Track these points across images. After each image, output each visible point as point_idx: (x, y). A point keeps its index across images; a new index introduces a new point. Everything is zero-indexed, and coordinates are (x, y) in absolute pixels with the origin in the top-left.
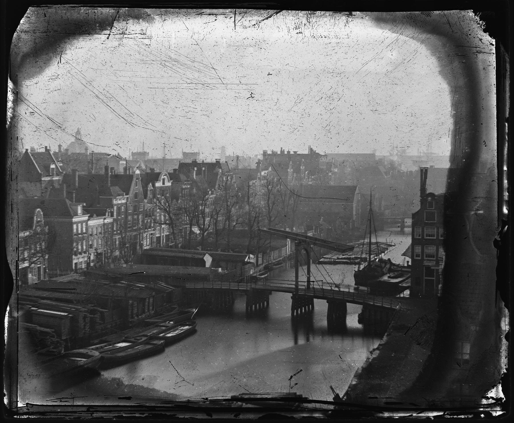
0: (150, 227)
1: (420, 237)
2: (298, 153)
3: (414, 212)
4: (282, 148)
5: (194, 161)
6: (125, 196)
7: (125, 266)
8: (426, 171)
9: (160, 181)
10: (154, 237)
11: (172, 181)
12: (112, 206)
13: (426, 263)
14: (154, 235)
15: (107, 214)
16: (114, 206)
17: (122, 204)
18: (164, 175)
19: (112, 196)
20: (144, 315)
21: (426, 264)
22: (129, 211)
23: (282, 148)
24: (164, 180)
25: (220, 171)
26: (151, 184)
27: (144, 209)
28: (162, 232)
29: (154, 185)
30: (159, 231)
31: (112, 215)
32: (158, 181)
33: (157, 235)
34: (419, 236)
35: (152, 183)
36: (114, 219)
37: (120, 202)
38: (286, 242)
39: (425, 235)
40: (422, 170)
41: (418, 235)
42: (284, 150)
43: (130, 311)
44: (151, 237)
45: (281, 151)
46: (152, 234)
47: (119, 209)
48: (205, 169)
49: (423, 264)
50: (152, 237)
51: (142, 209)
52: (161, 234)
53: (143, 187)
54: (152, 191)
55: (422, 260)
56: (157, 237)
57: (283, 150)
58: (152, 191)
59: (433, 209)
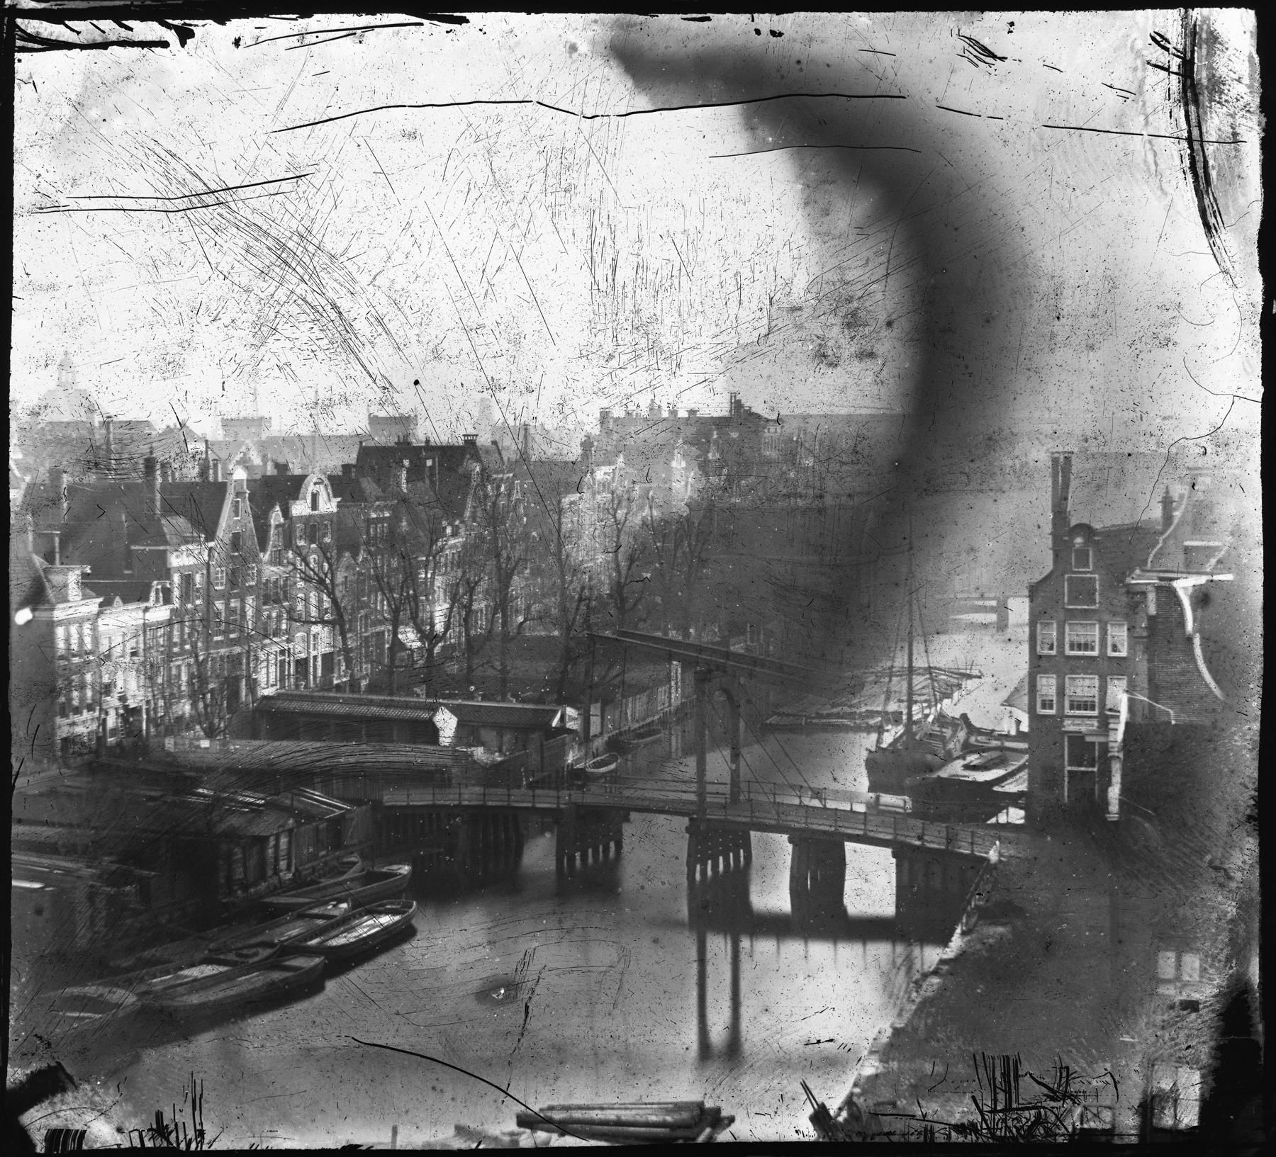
1: (1054, 652)
11: (339, 499)
12: (166, 573)
13: (1069, 726)
16: (172, 571)
18: (315, 484)
19: (166, 543)
21: (1072, 728)
26: (278, 508)
27: (259, 582)
29: (286, 512)
39: (1067, 646)
58: (280, 529)
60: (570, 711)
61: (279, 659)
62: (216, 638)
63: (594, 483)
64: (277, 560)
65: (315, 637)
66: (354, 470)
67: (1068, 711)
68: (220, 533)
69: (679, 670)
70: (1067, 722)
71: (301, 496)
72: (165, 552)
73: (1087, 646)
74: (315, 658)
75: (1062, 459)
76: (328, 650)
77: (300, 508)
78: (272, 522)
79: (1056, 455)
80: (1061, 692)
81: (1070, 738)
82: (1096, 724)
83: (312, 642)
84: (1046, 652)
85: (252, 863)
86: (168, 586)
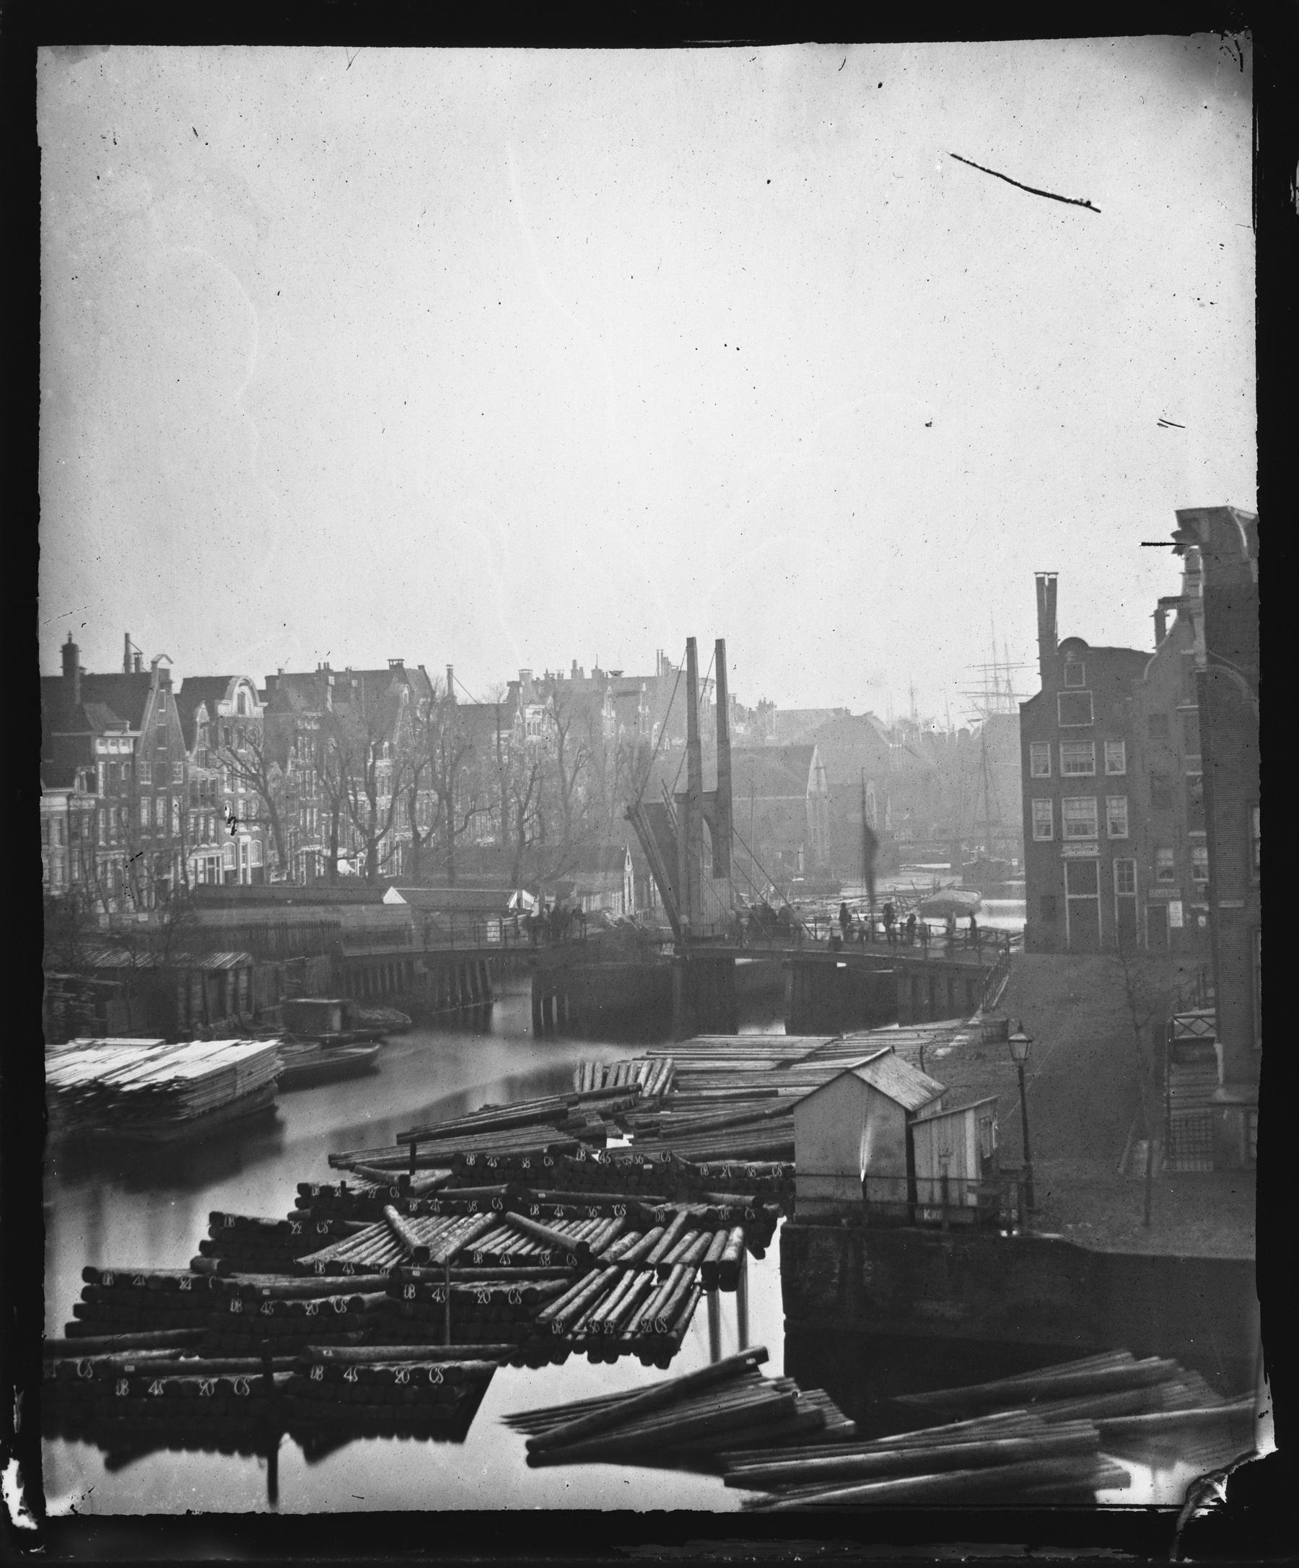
0: (206, 839)
1: (1049, 775)
2: (625, 675)
3: (1025, 700)
4: (575, 662)
5: (322, 668)
6: (131, 733)
7: (146, 919)
8: (1053, 582)
9: (231, 698)
10: (218, 871)
11: (265, 704)
12: (92, 759)
13: (1068, 852)
14: (218, 866)
15: (77, 782)
16: (96, 759)
17: (119, 756)
18: (241, 685)
19: (90, 728)
20: (224, 1021)
21: (1071, 854)
22: (142, 783)
23: (575, 662)
24: (242, 696)
25: (406, 691)
26: (203, 706)
27: (185, 782)
28: (241, 858)
29: (212, 711)
30: (232, 853)
31: (92, 787)
32: (223, 698)
33: (230, 867)
34: (1046, 771)
35: (206, 704)
36: (97, 800)
37: (113, 750)
38: (623, 879)
39: (1062, 768)
40: (1040, 581)
41: (1042, 768)
42: (581, 668)
43: (181, 1005)
44: (209, 869)
45: (574, 671)
46: (211, 860)
47: (112, 770)
48: (359, 684)
49: (1062, 855)
50: (214, 868)
51: (179, 779)
52: (238, 865)
53: (182, 717)
54: (206, 728)
55: (1059, 841)
56: (226, 873)
57: (578, 668)
58: (206, 728)
59: (1084, 685)
60: (527, 896)
61: (208, 867)
62: (144, 837)
63: (524, 721)
64: (205, 762)
65: (245, 848)
66: (278, 682)
67: (1065, 836)
68: (146, 724)
69: (632, 878)
70: (1066, 848)
71: (227, 694)
72: (88, 738)
73: (1082, 767)
74: (245, 870)
75: (1047, 583)
76: (257, 864)
77: (226, 709)
78: (198, 719)
79: (1042, 575)
80: (1058, 817)
81: (1069, 864)
82: (1097, 847)
83: (241, 855)
84: (1041, 775)
85: (212, 997)
86: (93, 772)
